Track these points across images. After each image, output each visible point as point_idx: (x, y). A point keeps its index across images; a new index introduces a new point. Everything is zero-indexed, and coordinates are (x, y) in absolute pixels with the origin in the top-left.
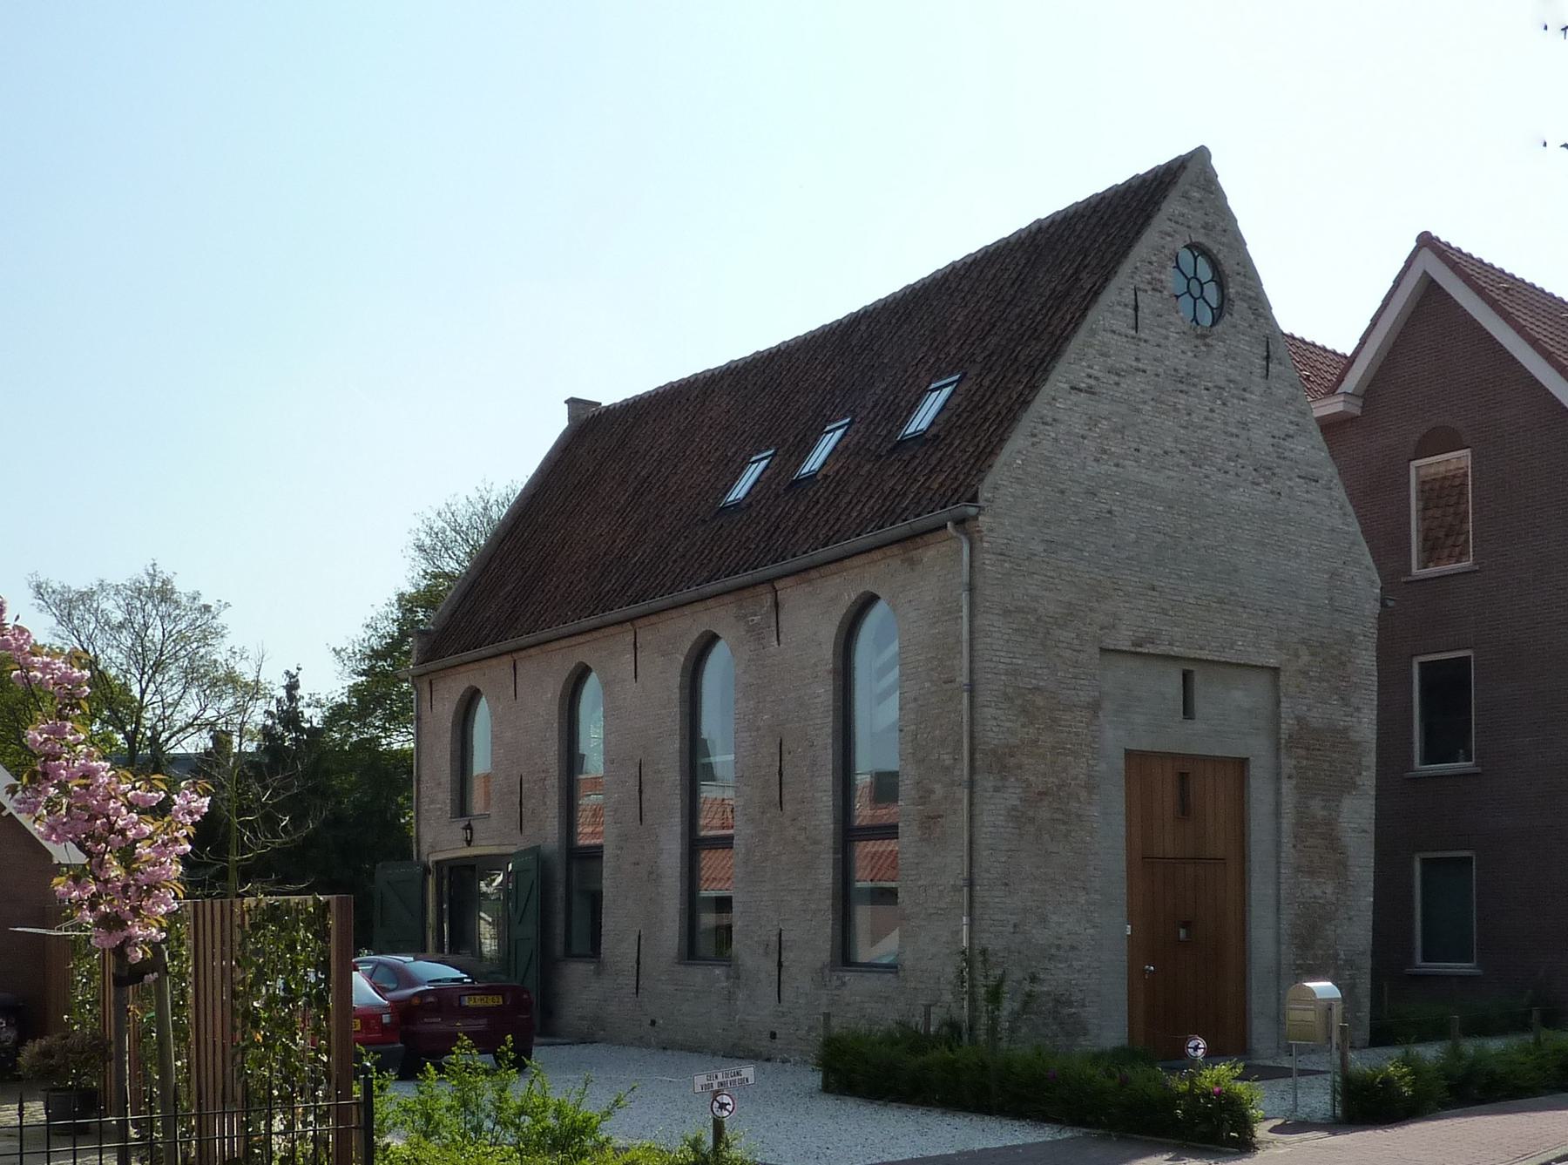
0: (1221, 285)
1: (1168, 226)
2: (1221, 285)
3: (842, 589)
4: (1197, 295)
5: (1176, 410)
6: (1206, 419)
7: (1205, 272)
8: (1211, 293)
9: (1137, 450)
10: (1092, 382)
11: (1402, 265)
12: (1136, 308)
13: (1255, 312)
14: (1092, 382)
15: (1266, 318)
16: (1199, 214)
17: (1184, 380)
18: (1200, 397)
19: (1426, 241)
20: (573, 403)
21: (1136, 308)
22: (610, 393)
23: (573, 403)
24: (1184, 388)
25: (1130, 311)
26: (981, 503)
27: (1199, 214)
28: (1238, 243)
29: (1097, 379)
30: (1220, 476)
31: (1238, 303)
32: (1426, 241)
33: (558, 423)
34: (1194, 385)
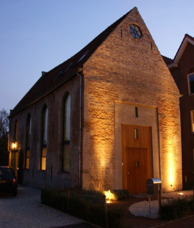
0: (141, 32)
1: (128, 19)
2: (141, 32)
3: (62, 92)
4: (136, 35)
5: (131, 54)
6: (138, 56)
7: (137, 29)
8: (139, 33)
9: (123, 61)
10: (111, 46)
11: (177, 51)
12: (121, 33)
13: (149, 38)
14: (111, 46)
15: (151, 39)
16: (135, 19)
17: (133, 48)
18: (137, 52)
19: (186, 35)
20: (42, 72)
21: (121, 33)
22: (47, 70)
23: (42, 72)
24: (133, 49)
25: (120, 34)
26: (83, 68)
27: (135, 19)
28: (144, 24)
29: (112, 46)
30: (142, 68)
31: (144, 35)
32: (186, 35)
33: (40, 75)
34: (135, 49)
